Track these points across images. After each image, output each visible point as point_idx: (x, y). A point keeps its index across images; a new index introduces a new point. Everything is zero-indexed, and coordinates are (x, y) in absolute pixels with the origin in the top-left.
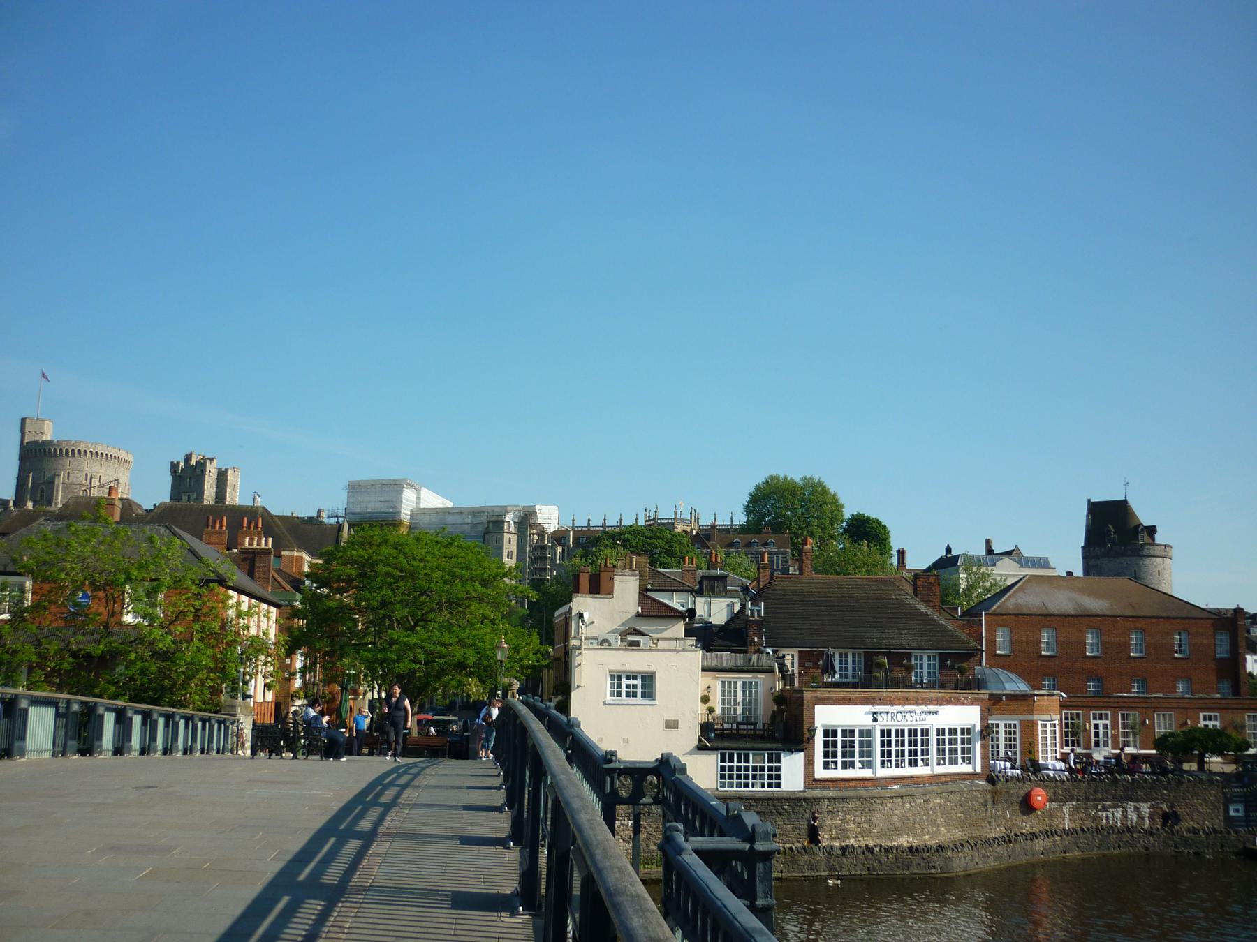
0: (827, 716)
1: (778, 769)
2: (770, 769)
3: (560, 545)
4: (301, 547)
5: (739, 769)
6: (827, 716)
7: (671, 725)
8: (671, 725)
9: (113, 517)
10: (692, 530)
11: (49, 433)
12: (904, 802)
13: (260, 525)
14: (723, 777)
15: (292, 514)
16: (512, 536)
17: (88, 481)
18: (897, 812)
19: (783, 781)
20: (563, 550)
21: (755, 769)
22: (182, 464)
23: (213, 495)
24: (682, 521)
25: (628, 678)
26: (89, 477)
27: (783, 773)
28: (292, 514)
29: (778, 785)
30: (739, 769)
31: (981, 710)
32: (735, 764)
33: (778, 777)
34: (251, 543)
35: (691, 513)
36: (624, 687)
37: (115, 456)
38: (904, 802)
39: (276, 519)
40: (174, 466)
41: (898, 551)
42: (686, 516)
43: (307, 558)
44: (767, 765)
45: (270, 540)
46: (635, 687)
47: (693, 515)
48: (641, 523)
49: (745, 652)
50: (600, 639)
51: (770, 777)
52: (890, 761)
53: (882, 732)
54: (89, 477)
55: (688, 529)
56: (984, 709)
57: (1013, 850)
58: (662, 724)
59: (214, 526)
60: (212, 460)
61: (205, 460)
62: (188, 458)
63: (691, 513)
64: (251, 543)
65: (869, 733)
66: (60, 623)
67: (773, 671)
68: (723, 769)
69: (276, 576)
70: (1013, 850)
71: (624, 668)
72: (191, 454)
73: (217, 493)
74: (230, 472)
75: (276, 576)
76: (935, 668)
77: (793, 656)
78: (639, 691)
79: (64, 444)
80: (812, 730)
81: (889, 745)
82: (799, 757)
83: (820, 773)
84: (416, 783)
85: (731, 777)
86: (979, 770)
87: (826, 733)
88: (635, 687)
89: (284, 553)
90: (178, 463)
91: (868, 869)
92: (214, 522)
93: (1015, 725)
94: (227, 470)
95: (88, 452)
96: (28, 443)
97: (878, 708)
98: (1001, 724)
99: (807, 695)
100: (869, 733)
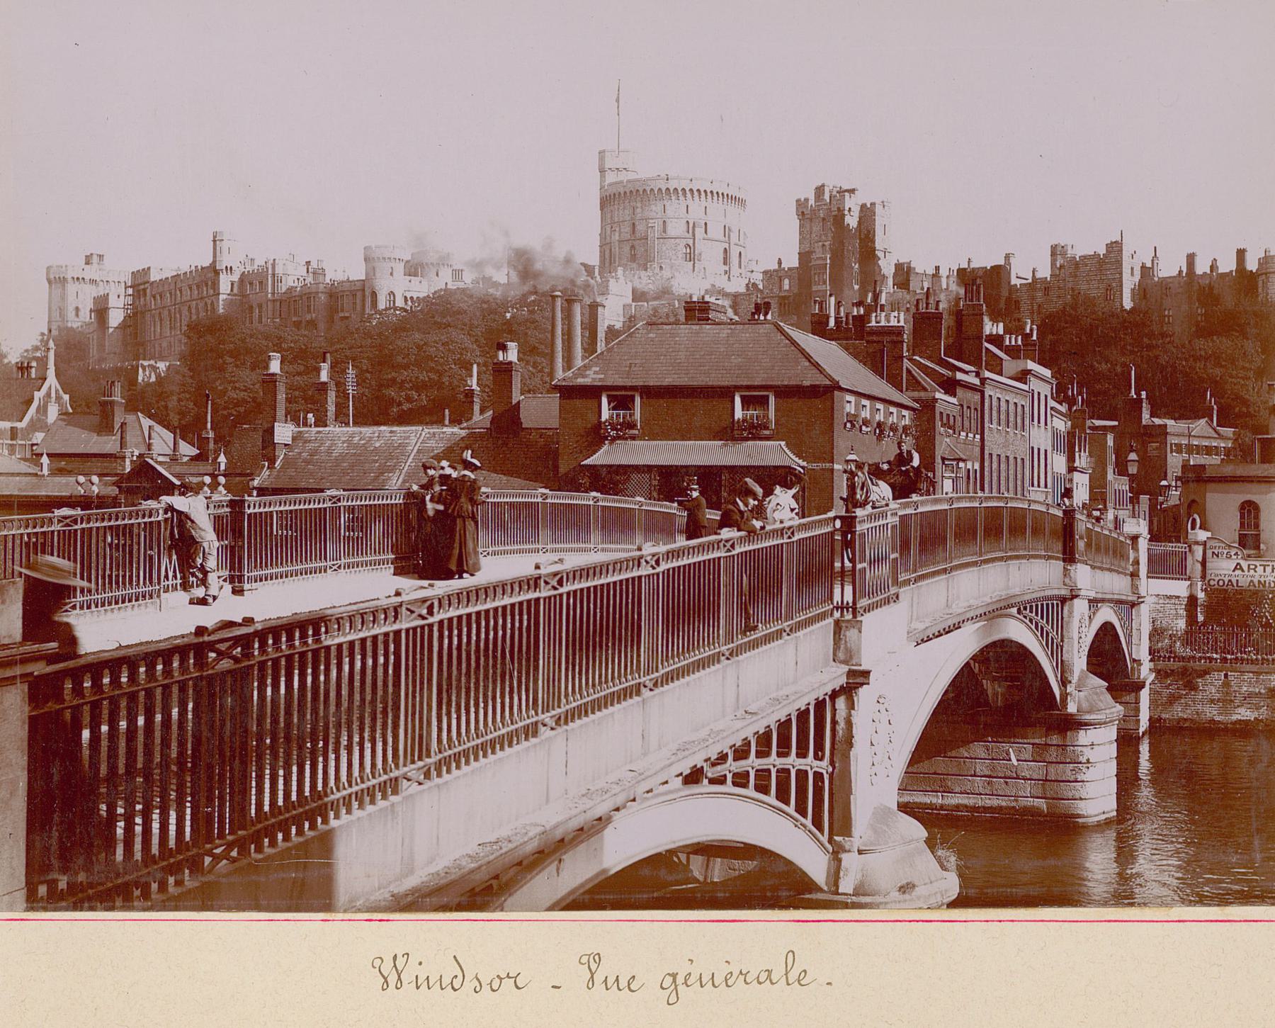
15: (780, 262)
17: (691, 231)
22: (812, 202)
26: (691, 225)
28: (780, 262)
32: (329, 563)
37: (712, 192)
45: (1020, 338)
54: (691, 225)
60: (852, 191)
61: (842, 192)
62: (820, 190)
66: (1212, 802)
72: (823, 186)
77: (260, 322)
84: (400, 969)
90: (807, 200)
94: (873, 204)
95: (687, 190)
96: (610, 185)
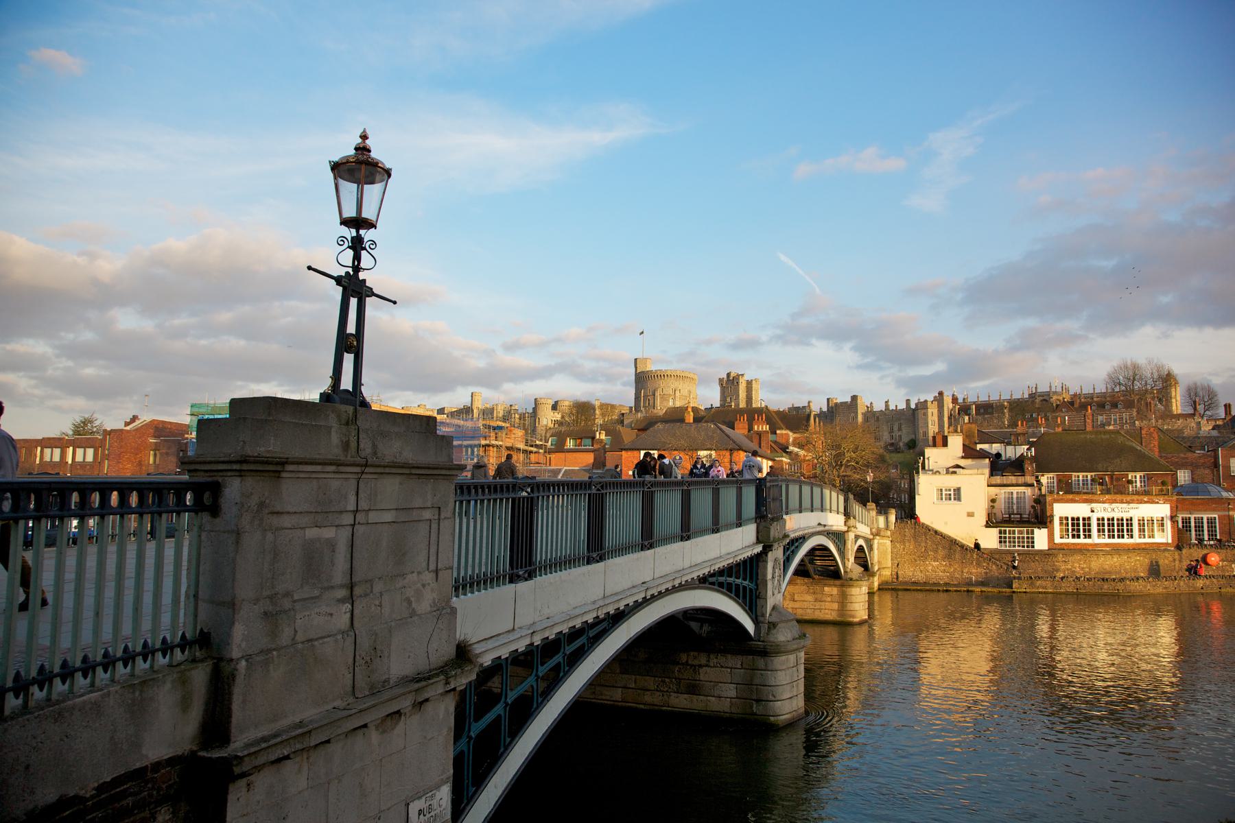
0: (1062, 510)
1: (1033, 538)
2: (1028, 538)
3: (966, 415)
4: (788, 428)
5: (1009, 538)
6: (1062, 510)
7: (970, 515)
8: (970, 515)
9: (849, 699)
10: (1064, 399)
11: (651, 367)
12: (1112, 558)
13: (764, 418)
14: (1000, 542)
16: (933, 410)
18: (1108, 563)
19: (1035, 544)
20: (969, 418)
21: (1019, 538)
23: (745, 396)
24: (1055, 393)
25: (946, 490)
27: (1035, 540)
29: (1033, 547)
30: (1009, 538)
31: (1171, 507)
33: (1033, 542)
34: (758, 428)
35: (1062, 387)
36: (944, 495)
38: (1112, 558)
39: (773, 414)
40: (721, 380)
41: (1225, 406)
42: (1059, 389)
43: (791, 434)
44: (1026, 536)
46: (950, 495)
47: (1064, 388)
48: (1026, 396)
49: (1024, 475)
50: (934, 471)
51: (1028, 542)
52: (1104, 535)
53: (1098, 519)
55: (1061, 398)
56: (1173, 505)
57: (1178, 584)
58: (966, 514)
59: (740, 420)
60: (743, 375)
61: (738, 375)
62: (728, 375)
63: (1062, 387)
64: (758, 428)
65: (1089, 518)
67: (1034, 486)
68: (1000, 537)
69: (773, 445)
70: (1178, 584)
71: (943, 486)
73: (747, 396)
74: (754, 382)
75: (773, 445)
76: (1144, 483)
78: (952, 497)
79: (659, 372)
80: (1052, 516)
81: (1127, 530)
82: (1044, 531)
83: (1058, 540)
85: (1005, 542)
86: (1170, 541)
87: (1061, 519)
88: (950, 495)
89: (778, 432)
91: (1077, 589)
92: (740, 418)
93: (1215, 518)
97: (1094, 505)
98: (1192, 517)
99: (1049, 499)
100: (1089, 518)
